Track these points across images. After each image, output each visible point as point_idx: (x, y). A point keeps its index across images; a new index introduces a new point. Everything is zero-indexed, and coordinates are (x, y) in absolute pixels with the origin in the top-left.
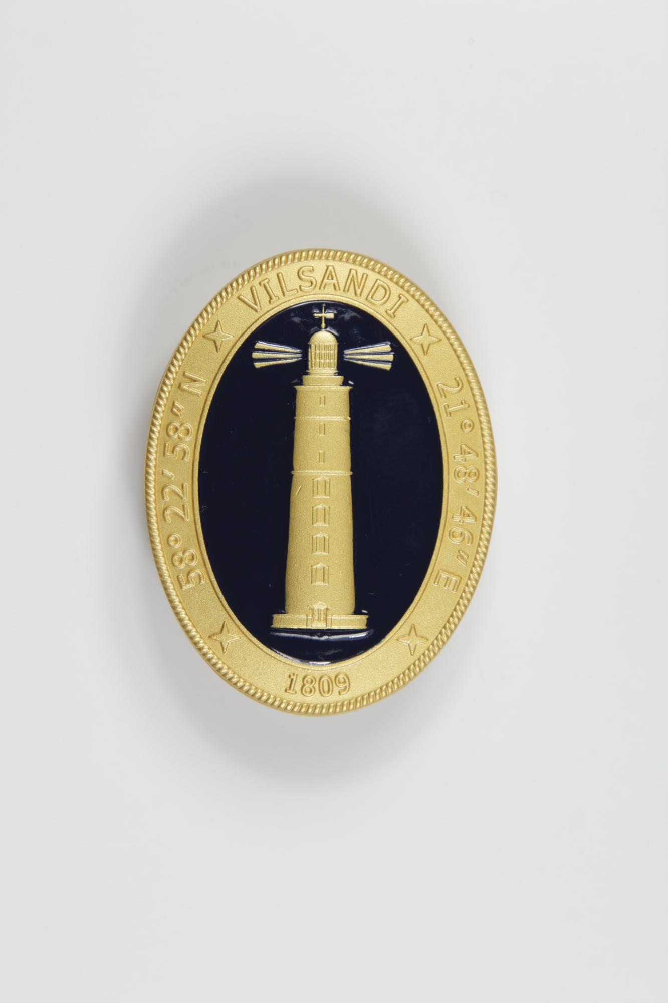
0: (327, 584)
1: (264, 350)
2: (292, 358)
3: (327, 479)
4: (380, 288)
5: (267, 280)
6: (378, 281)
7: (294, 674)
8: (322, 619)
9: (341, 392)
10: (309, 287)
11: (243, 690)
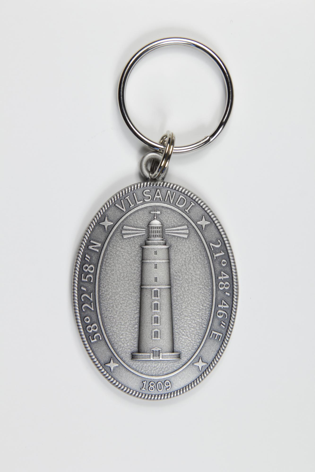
1: (184, 234)
4: (182, 199)
5: (129, 196)
6: (181, 196)
7: (144, 381)
8: (155, 352)
11: (105, 376)
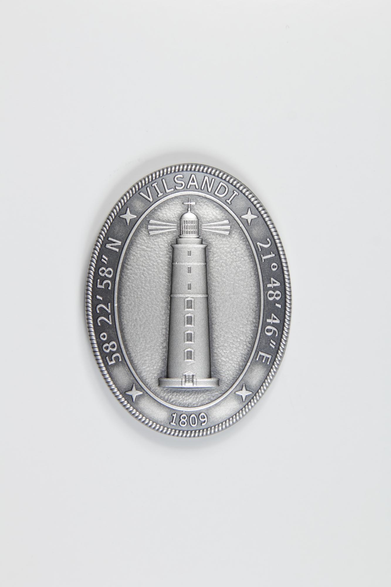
0: (194, 310)
1: (155, 225)
2: (173, 228)
3: (193, 299)
5: (156, 183)
9: (201, 265)
10: (181, 187)
